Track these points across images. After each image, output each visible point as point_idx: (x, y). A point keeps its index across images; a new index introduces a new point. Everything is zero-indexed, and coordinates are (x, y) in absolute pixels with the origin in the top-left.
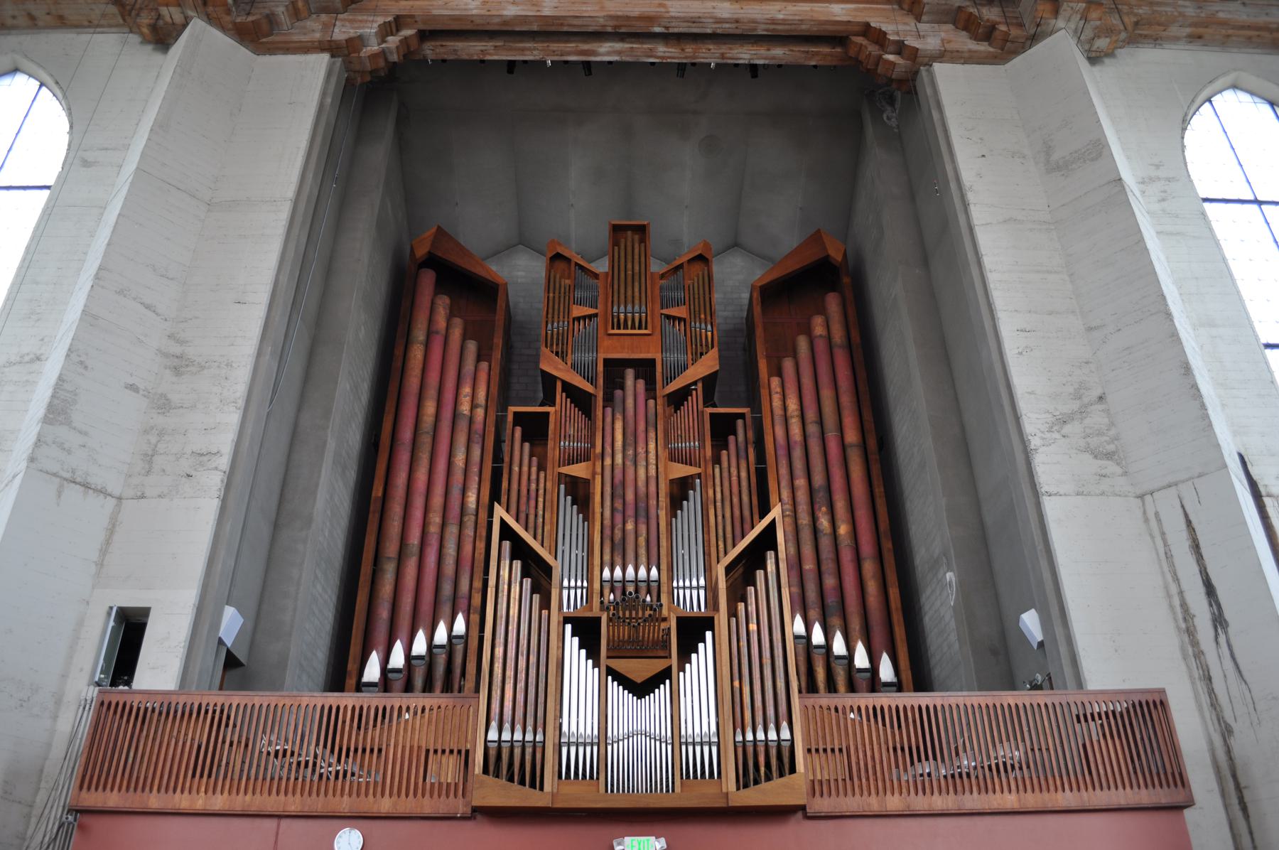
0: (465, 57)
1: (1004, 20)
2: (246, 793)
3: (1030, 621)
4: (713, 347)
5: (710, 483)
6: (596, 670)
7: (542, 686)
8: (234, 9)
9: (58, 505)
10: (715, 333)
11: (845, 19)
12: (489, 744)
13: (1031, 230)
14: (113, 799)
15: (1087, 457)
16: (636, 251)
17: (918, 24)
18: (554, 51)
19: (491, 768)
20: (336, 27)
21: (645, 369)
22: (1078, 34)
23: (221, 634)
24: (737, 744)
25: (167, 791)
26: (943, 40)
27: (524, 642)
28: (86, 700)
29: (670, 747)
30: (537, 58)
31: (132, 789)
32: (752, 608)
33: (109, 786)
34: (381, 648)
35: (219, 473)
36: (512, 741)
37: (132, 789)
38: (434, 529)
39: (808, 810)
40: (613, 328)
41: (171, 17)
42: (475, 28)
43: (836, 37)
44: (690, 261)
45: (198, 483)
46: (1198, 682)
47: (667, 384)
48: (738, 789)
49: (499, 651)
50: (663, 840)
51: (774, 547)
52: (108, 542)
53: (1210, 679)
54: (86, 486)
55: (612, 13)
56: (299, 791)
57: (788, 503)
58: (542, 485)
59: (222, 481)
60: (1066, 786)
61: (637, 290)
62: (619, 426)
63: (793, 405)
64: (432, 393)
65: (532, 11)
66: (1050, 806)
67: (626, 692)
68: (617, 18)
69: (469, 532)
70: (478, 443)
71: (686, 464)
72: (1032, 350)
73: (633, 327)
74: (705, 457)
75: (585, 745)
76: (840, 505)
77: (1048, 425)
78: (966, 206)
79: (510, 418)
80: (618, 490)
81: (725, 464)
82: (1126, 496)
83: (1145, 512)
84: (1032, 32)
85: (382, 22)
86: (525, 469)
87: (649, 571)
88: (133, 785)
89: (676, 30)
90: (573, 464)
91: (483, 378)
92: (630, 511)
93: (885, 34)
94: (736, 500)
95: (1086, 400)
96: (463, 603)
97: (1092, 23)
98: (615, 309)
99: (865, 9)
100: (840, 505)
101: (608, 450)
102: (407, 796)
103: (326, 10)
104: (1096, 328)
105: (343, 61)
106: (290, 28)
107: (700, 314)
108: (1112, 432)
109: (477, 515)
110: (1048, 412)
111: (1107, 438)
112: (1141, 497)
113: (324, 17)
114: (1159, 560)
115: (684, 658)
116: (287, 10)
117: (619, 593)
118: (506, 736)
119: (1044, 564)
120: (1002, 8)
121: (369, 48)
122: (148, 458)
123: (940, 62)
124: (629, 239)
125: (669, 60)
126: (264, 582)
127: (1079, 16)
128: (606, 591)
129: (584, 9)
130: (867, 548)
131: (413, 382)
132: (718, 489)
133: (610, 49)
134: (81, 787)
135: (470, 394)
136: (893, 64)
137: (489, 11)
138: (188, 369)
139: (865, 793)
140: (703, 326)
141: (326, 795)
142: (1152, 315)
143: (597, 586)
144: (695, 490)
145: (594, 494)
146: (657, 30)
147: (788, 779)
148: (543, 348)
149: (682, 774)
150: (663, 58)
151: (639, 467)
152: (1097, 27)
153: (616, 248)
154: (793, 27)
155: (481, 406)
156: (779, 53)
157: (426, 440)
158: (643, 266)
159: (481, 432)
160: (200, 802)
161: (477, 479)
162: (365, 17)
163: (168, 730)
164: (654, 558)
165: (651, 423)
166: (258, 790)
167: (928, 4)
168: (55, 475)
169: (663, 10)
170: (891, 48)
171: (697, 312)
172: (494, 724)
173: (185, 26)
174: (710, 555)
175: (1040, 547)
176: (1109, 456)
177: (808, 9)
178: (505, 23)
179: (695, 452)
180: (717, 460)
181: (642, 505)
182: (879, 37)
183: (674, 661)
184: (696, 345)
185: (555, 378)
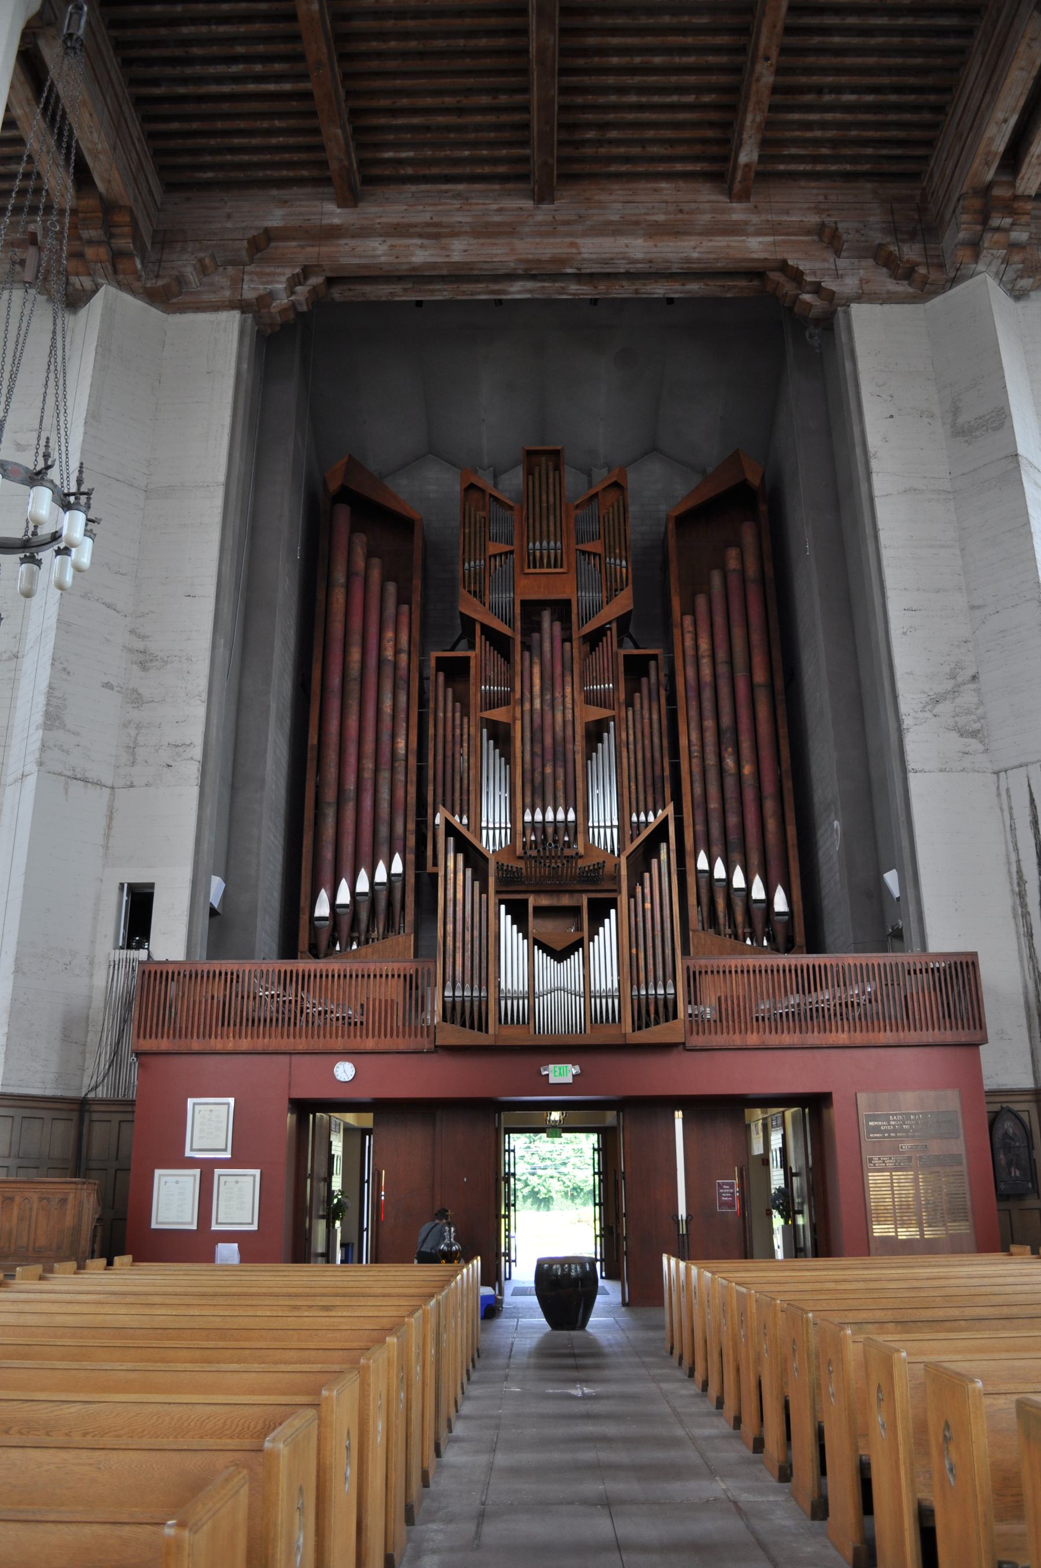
0: (373, 298)
3: (891, 878)
5: (624, 727)
6: (526, 941)
7: (484, 954)
15: (954, 735)
16: (551, 480)
17: (837, 260)
19: (449, 1017)
21: (562, 609)
23: (212, 900)
26: (861, 280)
29: (582, 999)
30: (447, 297)
31: (177, 1037)
32: (647, 890)
33: (160, 1035)
36: (463, 996)
37: (177, 1037)
38: (368, 775)
40: (529, 567)
42: (384, 274)
43: (756, 273)
46: (1022, 937)
48: (634, 1031)
49: (450, 927)
50: (577, 1067)
51: (667, 840)
53: (1031, 936)
54: (85, 780)
55: (523, 256)
56: (304, 1035)
58: (465, 730)
60: (888, 1028)
61: (552, 524)
63: (704, 645)
64: (356, 638)
65: (441, 256)
66: (873, 1042)
68: (528, 261)
69: (400, 777)
71: (601, 707)
73: (549, 566)
74: (619, 699)
75: (518, 998)
76: (746, 745)
78: (869, 473)
79: (433, 663)
81: (638, 706)
82: (984, 772)
83: (998, 788)
84: (952, 275)
86: (449, 714)
87: (566, 813)
88: (177, 1034)
89: (588, 271)
90: (494, 708)
91: (404, 620)
92: (549, 756)
93: (802, 273)
94: (647, 742)
95: (960, 679)
96: (399, 844)
97: (1013, 266)
98: (531, 545)
99: (784, 242)
100: (746, 745)
101: (527, 695)
102: (385, 1036)
103: (233, 263)
104: (979, 607)
105: (254, 317)
107: (615, 549)
108: (980, 711)
110: (924, 692)
112: (997, 773)
113: (230, 270)
115: (594, 932)
116: (195, 269)
117: (539, 833)
118: (458, 993)
120: (925, 243)
121: (279, 301)
125: (581, 297)
127: (1000, 261)
128: (528, 831)
129: (494, 252)
130: (769, 788)
132: (631, 732)
133: (521, 288)
134: (138, 1037)
136: (810, 306)
138: (153, 664)
139: (731, 1032)
144: (608, 732)
145: (514, 737)
146: (569, 271)
147: (672, 1023)
148: (461, 589)
153: (530, 477)
154: (708, 265)
156: (694, 287)
157: (354, 687)
158: (558, 496)
159: (405, 677)
160: (230, 1045)
161: (404, 725)
162: (272, 269)
163: (198, 991)
165: (567, 667)
168: (60, 774)
169: (574, 251)
170: (808, 288)
173: (95, 292)
175: (902, 818)
176: (974, 734)
177: (724, 244)
178: (414, 269)
179: (609, 696)
180: (630, 703)
181: (560, 749)
182: (796, 276)
184: (611, 582)
185: (473, 621)
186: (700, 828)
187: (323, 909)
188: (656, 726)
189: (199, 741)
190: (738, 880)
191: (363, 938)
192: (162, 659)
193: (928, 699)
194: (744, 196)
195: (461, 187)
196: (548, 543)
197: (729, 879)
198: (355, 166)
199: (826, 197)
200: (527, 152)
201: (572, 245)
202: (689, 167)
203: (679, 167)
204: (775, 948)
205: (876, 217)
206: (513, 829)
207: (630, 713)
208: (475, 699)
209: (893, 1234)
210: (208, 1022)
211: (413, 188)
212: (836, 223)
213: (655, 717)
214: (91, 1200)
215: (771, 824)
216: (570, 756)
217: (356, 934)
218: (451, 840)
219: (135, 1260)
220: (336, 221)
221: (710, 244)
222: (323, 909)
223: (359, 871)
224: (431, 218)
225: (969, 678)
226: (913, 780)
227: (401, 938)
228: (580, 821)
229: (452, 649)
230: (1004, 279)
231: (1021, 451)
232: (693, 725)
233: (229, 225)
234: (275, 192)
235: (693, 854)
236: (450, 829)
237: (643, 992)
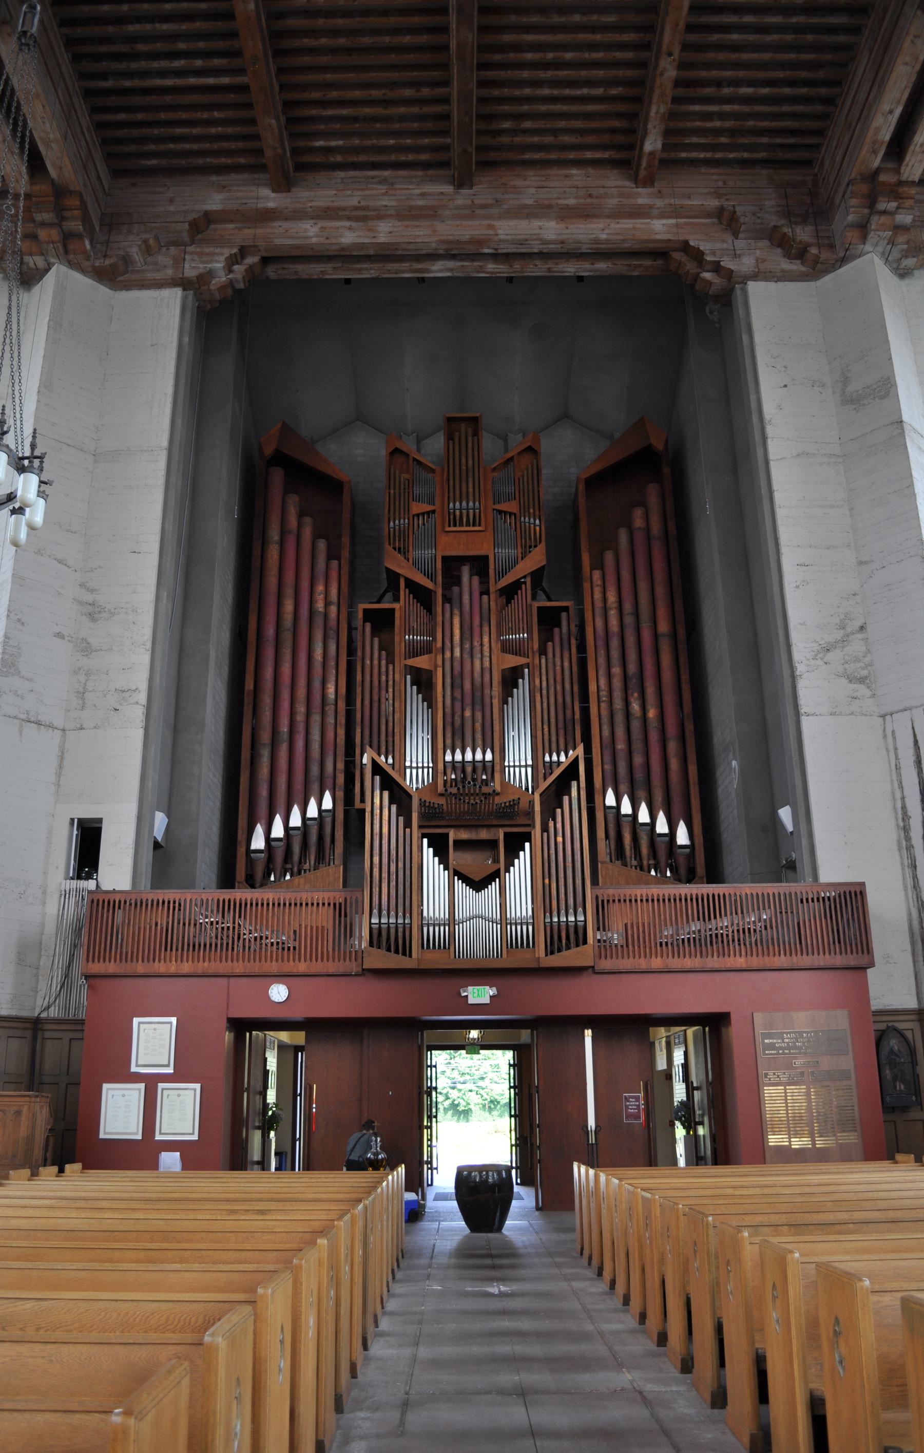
1: (816, 241)
2: (204, 961)
3: (785, 814)
5: (537, 673)
6: (446, 872)
7: (408, 884)
8: (92, 253)
9: (21, 741)
10: (543, 528)
14: (111, 967)
15: (844, 681)
16: (470, 445)
17: (735, 240)
18: (389, 270)
19: (375, 942)
21: (480, 565)
24: (547, 924)
25: (148, 961)
26: (757, 259)
27: (393, 852)
28: (65, 891)
29: (499, 926)
32: (559, 825)
33: (107, 959)
35: (140, 707)
36: (388, 923)
38: (300, 718)
39: (596, 968)
40: (450, 526)
41: (35, 264)
43: (660, 253)
44: (519, 453)
46: (906, 868)
48: (546, 955)
49: (376, 859)
50: (494, 989)
51: (577, 778)
52: (61, 766)
54: (38, 723)
55: (444, 238)
56: (241, 959)
57: (604, 690)
58: (391, 677)
60: (782, 952)
61: (471, 485)
62: (457, 621)
63: (612, 598)
64: (289, 591)
66: (768, 966)
67: (468, 887)
69: (331, 720)
70: (333, 639)
71: (516, 655)
73: (468, 525)
74: (533, 648)
75: (439, 925)
76: (650, 691)
77: (813, 653)
79: (360, 615)
81: (550, 655)
83: (884, 730)
84: (841, 254)
85: (228, 255)
86: (376, 662)
87: (484, 753)
89: (504, 251)
90: (417, 656)
91: (334, 575)
92: (468, 700)
93: (702, 253)
94: (559, 688)
95: (849, 630)
96: (329, 782)
97: (899, 246)
98: (451, 505)
100: (650, 691)
101: (448, 644)
103: (175, 244)
104: (866, 563)
105: (195, 294)
106: (143, 264)
107: (529, 509)
109: (336, 705)
111: (863, 665)
112: (883, 716)
114: (891, 771)
115: (509, 864)
116: (140, 249)
117: (459, 772)
118: (384, 920)
120: (816, 225)
122: (81, 695)
123: (755, 281)
124: (463, 432)
125: (498, 275)
126: (172, 782)
127: (886, 242)
128: (449, 771)
129: (417, 233)
130: (672, 730)
131: (272, 581)
132: (544, 678)
134: (88, 961)
135: (324, 592)
136: (710, 283)
137: (327, 238)
138: (101, 616)
140: (532, 520)
141: (260, 961)
142: (911, 557)
143: (441, 766)
144: (523, 679)
145: (436, 683)
146: (487, 251)
147: (582, 948)
148: (387, 546)
149: (507, 945)
150: (492, 273)
151: (475, 659)
152: (903, 250)
154: (616, 246)
155: (334, 604)
156: (603, 266)
157: (287, 636)
158: (476, 460)
159: (335, 628)
160: (173, 968)
162: (211, 249)
165: (485, 618)
166: (212, 959)
167: (744, 224)
168: (15, 717)
169: (491, 232)
170: (708, 267)
171: (526, 507)
173: (47, 270)
174: (536, 737)
175: (795, 758)
176: (862, 680)
177: (630, 226)
178: (343, 249)
179: (524, 645)
180: (543, 651)
181: (478, 694)
182: (697, 256)
184: (526, 539)
185: (397, 576)
186: (608, 767)
187: (258, 842)
188: (567, 672)
189: (144, 686)
190: (644, 816)
191: (295, 869)
192: (109, 611)
194: (649, 182)
195: (386, 173)
196: (468, 504)
198: (288, 154)
199: (725, 183)
201: (490, 227)
202: (598, 155)
203: (589, 155)
205: (771, 202)
207: (543, 661)
208: (399, 648)
209: (787, 1144)
211: (342, 174)
212: (734, 206)
213: (566, 664)
214: (44, 1112)
215: (674, 764)
216: (487, 700)
217: (289, 866)
218: (377, 778)
219: (84, 1168)
220: (271, 205)
224: (359, 202)
226: (806, 723)
227: (331, 869)
228: (497, 760)
231: (905, 417)
232: (602, 672)
233: (172, 208)
234: (214, 178)
236: (377, 768)
237: (555, 919)
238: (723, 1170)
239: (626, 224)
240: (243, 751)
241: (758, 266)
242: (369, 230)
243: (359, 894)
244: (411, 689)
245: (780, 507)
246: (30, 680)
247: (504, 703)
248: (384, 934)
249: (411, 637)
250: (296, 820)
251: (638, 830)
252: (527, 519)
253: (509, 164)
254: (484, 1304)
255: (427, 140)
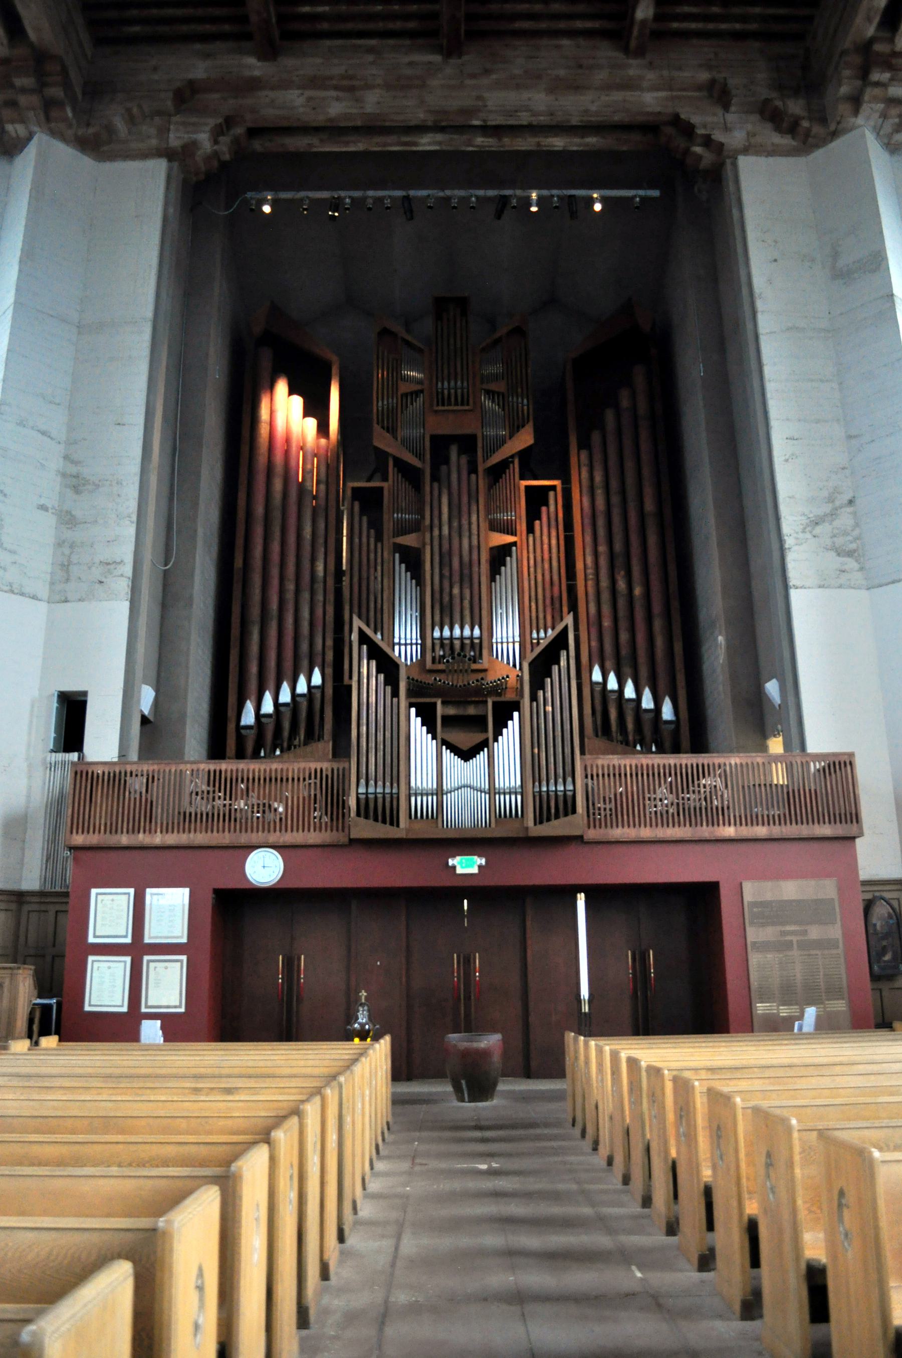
3: (772, 688)
4: (528, 421)
6: (434, 741)
11: (658, 109)
12: (360, 796)
13: (811, 338)
15: (833, 554)
19: (362, 812)
20: (171, 132)
21: (468, 444)
22: (877, 131)
26: (748, 134)
28: (51, 764)
32: (549, 695)
34: (253, 697)
35: (125, 579)
36: (375, 793)
38: (290, 596)
39: (585, 837)
40: (438, 405)
45: (109, 588)
47: (487, 459)
48: (535, 824)
51: (566, 648)
58: (379, 554)
59: (128, 586)
69: (320, 597)
72: (797, 457)
73: (456, 404)
77: (802, 527)
79: (349, 493)
80: (445, 559)
84: (832, 127)
86: (364, 540)
87: (472, 630)
89: (494, 123)
92: (456, 578)
94: (547, 566)
95: (837, 503)
96: (319, 659)
98: (440, 385)
101: (436, 522)
103: (159, 113)
104: (855, 437)
110: (804, 514)
111: (850, 538)
115: (498, 733)
117: (447, 648)
118: (371, 790)
119: (785, 644)
122: (65, 568)
125: (487, 149)
127: (878, 114)
128: (437, 647)
130: (657, 608)
136: (700, 158)
146: (476, 123)
147: (570, 818)
148: (375, 425)
156: (592, 141)
164: (477, 619)
169: (480, 103)
172: (363, 781)
173: (29, 138)
175: (784, 630)
176: (850, 554)
178: (331, 120)
180: (530, 530)
181: (466, 572)
182: (688, 130)
183: (490, 734)
185: (386, 454)
186: (594, 644)
187: (248, 717)
188: (554, 550)
189: (129, 559)
190: (629, 692)
191: (285, 745)
192: (94, 483)
193: (808, 521)
194: (640, 52)
195: (373, 42)
196: (456, 383)
197: (621, 690)
198: (274, 20)
199: (716, 54)
200: (437, 7)
201: (479, 98)
202: (589, 25)
203: (579, 24)
204: (661, 750)
205: (762, 76)
206: (423, 646)
208: (388, 526)
209: (775, 1011)
210: (137, 818)
211: (328, 43)
212: (725, 79)
213: (554, 542)
214: (27, 984)
215: (659, 642)
216: (475, 577)
217: (279, 742)
219: (60, 1040)
220: (257, 73)
221: (607, 98)
222: (248, 717)
223: (282, 683)
224: (346, 71)
225: (846, 502)
226: (794, 594)
227: (320, 745)
228: (485, 637)
229: (369, 480)
230: (882, 133)
231: (895, 292)
232: (589, 550)
233: (156, 77)
234: (198, 46)
235: (588, 668)
236: (364, 638)
237: (544, 789)
238: (832, 1052)
239: (617, 96)
240: (233, 631)
241: (748, 140)
242: (357, 100)
243: (346, 765)
244: (400, 568)
245: (770, 381)
246: (13, 552)
247: (491, 581)
248: (372, 805)
249: (400, 515)
250: (285, 696)
251: (624, 706)
252: (515, 399)
253: (500, 34)
254: (473, 1184)
255: (415, 7)
